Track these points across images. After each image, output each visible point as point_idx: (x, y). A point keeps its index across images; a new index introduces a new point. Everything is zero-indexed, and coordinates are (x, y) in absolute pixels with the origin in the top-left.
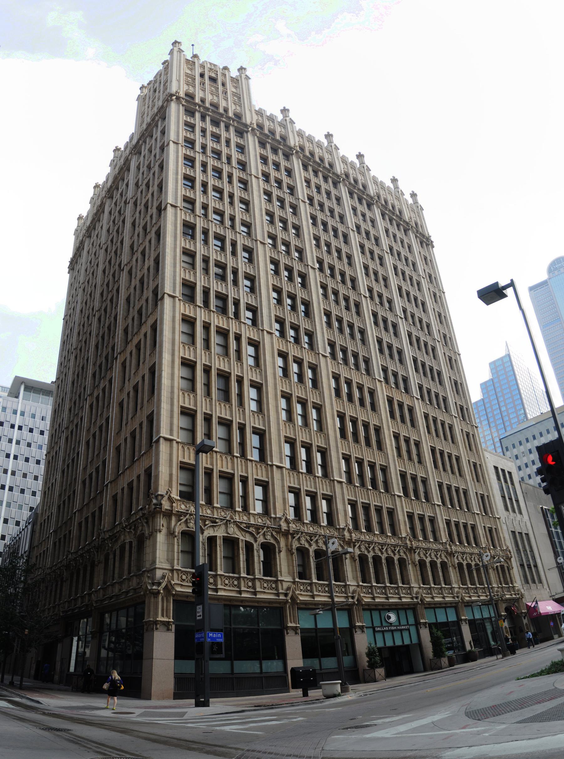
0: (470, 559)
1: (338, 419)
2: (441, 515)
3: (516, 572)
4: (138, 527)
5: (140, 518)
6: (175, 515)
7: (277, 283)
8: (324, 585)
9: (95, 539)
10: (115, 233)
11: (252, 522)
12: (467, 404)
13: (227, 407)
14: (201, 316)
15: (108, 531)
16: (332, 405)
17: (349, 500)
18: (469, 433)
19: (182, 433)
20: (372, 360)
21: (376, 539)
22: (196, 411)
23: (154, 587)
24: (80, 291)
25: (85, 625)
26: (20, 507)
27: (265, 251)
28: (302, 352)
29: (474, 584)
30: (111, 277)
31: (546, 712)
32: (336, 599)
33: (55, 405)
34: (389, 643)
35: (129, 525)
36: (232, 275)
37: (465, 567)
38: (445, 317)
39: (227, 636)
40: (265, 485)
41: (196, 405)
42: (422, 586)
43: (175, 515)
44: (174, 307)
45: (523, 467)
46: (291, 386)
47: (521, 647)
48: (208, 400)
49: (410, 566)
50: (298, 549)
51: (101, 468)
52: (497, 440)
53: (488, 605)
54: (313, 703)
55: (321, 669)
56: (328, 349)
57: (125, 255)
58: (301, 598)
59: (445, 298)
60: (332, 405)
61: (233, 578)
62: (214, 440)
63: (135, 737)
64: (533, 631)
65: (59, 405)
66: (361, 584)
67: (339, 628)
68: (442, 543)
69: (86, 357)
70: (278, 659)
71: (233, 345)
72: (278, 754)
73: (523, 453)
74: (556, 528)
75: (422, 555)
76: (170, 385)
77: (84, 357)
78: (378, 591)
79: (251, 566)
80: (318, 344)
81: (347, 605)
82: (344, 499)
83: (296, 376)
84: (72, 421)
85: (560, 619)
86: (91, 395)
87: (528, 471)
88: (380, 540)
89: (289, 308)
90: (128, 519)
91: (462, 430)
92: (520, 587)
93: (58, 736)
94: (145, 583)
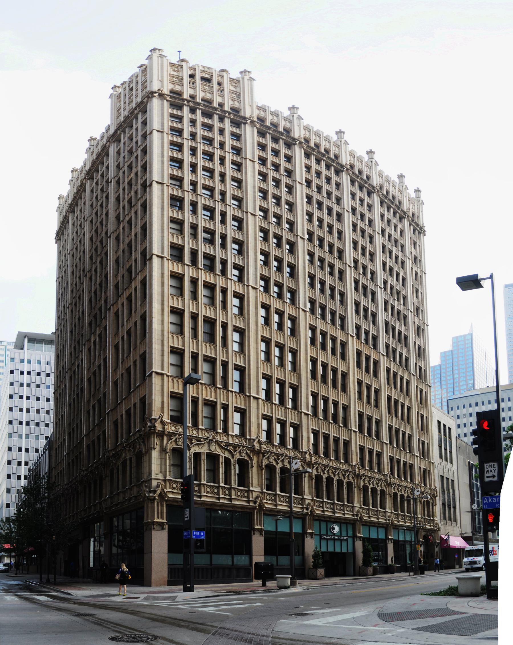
0: (404, 491)
1: (311, 363)
2: (387, 451)
3: (438, 509)
4: (136, 446)
5: (137, 439)
6: (166, 435)
7: (265, 248)
8: (286, 496)
9: (102, 458)
10: (99, 207)
11: (231, 441)
12: (426, 366)
13: (212, 347)
14: (189, 273)
15: (111, 451)
16: (306, 350)
17: (312, 429)
18: (423, 415)
19: (171, 368)
20: (348, 318)
21: (331, 464)
22: (184, 350)
23: (151, 495)
24: (70, 257)
25: (99, 528)
26: (37, 437)
27: (255, 221)
28: (283, 305)
29: (404, 512)
30: (98, 243)
31: (436, 625)
32: (294, 509)
33: (57, 352)
34: (331, 549)
35: (128, 444)
36: (220, 266)
37: (399, 497)
38: (421, 293)
39: (207, 534)
40: (243, 412)
41: (184, 345)
42: (362, 506)
43: (166, 435)
44: (163, 265)
45: (462, 426)
46: (271, 333)
47: (429, 570)
48: (195, 342)
49: (356, 489)
50: (267, 466)
51: (102, 400)
52: (445, 400)
53: (411, 530)
54: (270, 592)
55: (277, 565)
56: (309, 305)
57: (111, 224)
58: (267, 506)
59: (425, 278)
60: (306, 350)
61: (213, 486)
62: (200, 374)
63: (141, 617)
64: (441, 558)
65: (61, 351)
66: (315, 498)
67: (294, 533)
68: (384, 475)
69: (81, 310)
70: (246, 554)
71: (219, 297)
72: (241, 632)
73: (465, 415)
74: (476, 481)
75: (366, 482)
76: (160, 329)
77: (79, 310)
78: (328, 506)
79: (228, 474)
80: (299, 301)
81: (302, 514)
82: (308, 428)
83: (276, 325)
84: (74, 363)
85: (463, 553)
86: (89, 340)
87: (465, 430)
88: (335, 465)
89: (275, 269)
90: (127, 440)
91: (417, 386)
92: (439, 522)
93: (86, 620)
94: (144, 491)
